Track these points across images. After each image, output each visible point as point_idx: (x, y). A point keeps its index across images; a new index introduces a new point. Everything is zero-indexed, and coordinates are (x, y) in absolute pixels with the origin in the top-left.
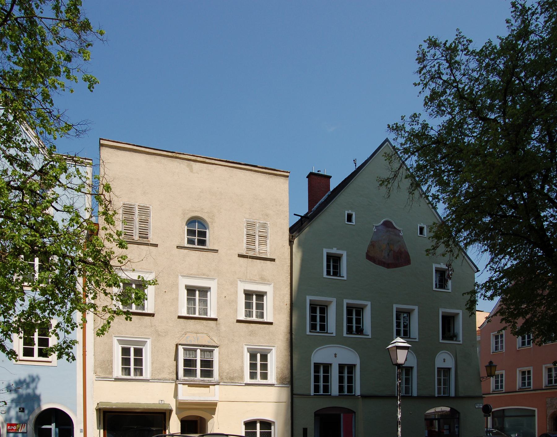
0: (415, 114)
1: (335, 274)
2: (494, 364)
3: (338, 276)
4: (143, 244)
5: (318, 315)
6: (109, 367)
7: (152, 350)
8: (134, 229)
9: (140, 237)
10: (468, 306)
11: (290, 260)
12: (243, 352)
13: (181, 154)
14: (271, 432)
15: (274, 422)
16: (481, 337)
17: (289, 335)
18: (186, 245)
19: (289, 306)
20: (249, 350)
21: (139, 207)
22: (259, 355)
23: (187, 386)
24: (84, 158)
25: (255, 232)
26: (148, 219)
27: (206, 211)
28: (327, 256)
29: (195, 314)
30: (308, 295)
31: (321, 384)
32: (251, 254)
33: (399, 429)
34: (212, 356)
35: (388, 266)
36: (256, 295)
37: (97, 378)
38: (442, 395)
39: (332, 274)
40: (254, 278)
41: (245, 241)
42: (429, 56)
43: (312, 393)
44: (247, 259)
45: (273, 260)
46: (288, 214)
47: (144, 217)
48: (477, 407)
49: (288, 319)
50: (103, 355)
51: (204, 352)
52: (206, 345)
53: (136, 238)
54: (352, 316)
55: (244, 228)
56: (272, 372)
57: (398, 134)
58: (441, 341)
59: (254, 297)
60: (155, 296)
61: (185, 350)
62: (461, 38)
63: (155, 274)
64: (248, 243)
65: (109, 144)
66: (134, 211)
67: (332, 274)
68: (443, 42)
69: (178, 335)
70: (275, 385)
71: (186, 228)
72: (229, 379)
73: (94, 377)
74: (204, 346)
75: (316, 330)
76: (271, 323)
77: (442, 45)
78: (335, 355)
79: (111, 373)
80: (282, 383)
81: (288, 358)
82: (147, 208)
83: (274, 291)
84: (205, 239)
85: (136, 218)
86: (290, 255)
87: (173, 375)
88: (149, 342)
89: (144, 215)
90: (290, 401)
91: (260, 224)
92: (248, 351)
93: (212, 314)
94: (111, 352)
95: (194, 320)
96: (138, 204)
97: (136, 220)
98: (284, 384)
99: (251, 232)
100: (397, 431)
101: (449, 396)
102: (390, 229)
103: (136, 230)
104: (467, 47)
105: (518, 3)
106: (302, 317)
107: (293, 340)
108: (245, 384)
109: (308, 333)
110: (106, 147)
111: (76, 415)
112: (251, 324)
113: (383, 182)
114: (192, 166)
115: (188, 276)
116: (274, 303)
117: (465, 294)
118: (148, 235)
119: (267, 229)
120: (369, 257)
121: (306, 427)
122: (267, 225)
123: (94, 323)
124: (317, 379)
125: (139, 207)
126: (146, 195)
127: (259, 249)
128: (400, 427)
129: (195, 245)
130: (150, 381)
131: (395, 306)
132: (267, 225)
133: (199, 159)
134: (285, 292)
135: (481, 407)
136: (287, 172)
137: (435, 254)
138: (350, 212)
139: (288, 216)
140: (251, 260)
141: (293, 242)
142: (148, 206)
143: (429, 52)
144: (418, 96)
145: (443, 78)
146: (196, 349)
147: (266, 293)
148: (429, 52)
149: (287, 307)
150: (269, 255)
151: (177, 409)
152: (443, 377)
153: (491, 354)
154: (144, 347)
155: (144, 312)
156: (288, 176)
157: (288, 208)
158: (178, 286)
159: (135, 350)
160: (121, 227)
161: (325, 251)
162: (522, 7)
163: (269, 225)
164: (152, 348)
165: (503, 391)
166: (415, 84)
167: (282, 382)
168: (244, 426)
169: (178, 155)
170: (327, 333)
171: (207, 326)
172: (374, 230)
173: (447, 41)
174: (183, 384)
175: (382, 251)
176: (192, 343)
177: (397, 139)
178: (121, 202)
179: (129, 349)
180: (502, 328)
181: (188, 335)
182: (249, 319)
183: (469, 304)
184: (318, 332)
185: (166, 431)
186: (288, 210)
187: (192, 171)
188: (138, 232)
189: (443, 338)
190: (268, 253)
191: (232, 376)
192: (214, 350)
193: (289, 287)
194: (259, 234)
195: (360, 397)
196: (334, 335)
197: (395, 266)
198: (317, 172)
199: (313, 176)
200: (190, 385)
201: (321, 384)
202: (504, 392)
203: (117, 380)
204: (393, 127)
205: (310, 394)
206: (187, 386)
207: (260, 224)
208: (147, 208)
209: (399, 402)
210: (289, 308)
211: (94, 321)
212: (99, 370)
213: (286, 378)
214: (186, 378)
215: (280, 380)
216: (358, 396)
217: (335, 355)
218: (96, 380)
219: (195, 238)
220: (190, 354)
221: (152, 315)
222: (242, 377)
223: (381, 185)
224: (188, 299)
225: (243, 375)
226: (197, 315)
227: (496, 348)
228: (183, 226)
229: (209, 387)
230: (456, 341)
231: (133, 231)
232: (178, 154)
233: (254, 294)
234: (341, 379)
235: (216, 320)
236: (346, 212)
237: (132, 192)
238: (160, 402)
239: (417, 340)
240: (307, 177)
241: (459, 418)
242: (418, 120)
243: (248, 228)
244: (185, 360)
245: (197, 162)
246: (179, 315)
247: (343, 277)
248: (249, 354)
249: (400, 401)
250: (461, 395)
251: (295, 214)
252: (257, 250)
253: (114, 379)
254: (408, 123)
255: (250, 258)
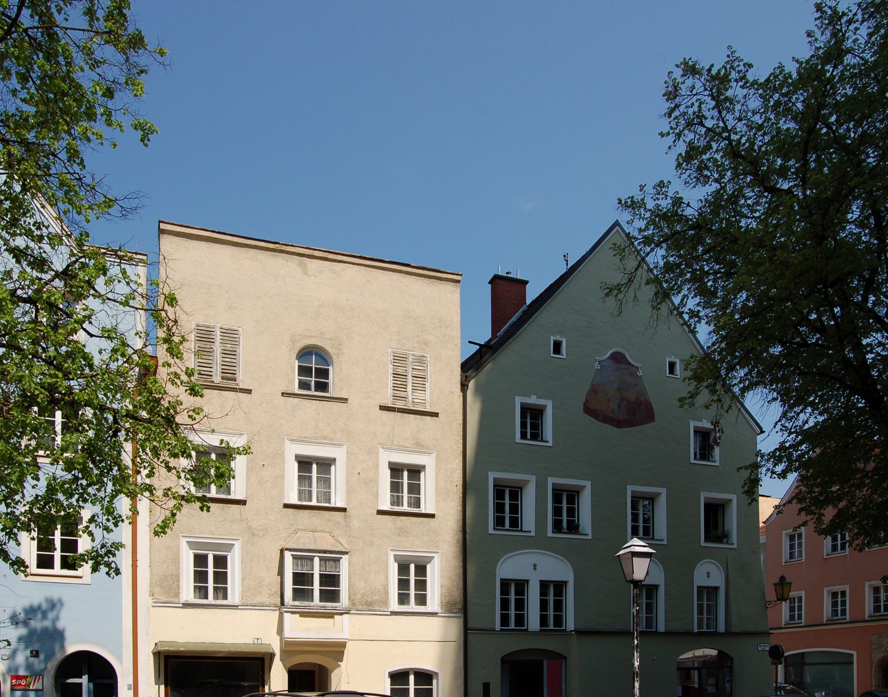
0: (662, 182)
1: (534, 437)
2: (788, 580)
3: (539, 441)
5: (507, 502)
10: (746, 488)
11: (462, 414)
14: (432, 689)
16: (766, 538)
28: (521, 408)
30: (492, 470)
31: (512, 612)
33: (637, 685)
35: (618, 424)
38: (705, 630)
39: (529, 437)
42: (684, 90)
43: (498, 627)
45: (436, 415)
46: (459, 341)
48: (760, 649)
49: (460, 508)
54: (561, 504)
57: (635, 213)
58: (703, 544)
62: (735, 60)
67: (529, 437)
68: (707, 67)
70: (439, 615)
75: (504, 527)
77: (705, 72)
78: (535, 565)
81: (460, 571)
86: (462, 407)
98: (453, 612)
100: (634, 687)
101: (716, 631)
102: (622, 366)
104: (745, 75)
105: (826, 5)
106: (481, 506)
107: (468, 543)
109: (491, 531)
113: (611, 290)
117: (741, 468)
120: (588, 410)
121: (488, 681)
122: (425, 359)
124: (505, 604)
128: (637, 681)
131: (630, 489)
132: (425, 359)
135: (768, 649)
136: (458, 275)
137: (694, 405)
138: (558, 338)
139: (459, 345)
141: (468, 386)
143: (684, 83)
144: (667, 153)
145: (706, 125)
148: (684, 83)
149: (457, 490)
152: (707, 601)
153: (783, 564)
156: (458, 281)
161: (518, 401)
162: (832, 11)
165: (801, 623)
166: (662, 135)
167: (450, 610)
170: (521, 531)
172: (597, 366)
173: (712, 66)
175: (609, 401)
177: (633, 222)
180: (801, 523)
183: (747, 485)
184: (507, 530)
186: (459, 335)
189: (707, 539)
195: (574, 633)
196: (533, 534)
197: (630, 424)
198: (506, 275)
199: (499, 281)
201: (512, 612)
202: (803, 624)
204: (626, 202)
205: (495, 628)
209: (636, 642)
210: (461, 492)
215: (446, 606)
216: (571, 631)
217: (535, 565)
223: (607, 295)
227: (792, 556)
230: (727, 543)
234: (544, 605)
236: (552, 339)
239: (665, 543)
240: (490, 283)
241: (731, 667)
242: (667, 192)
247: (547, 442)
249: (637, 640)
250: (735, 630)
251: (470, 342)
254: (651, 196)
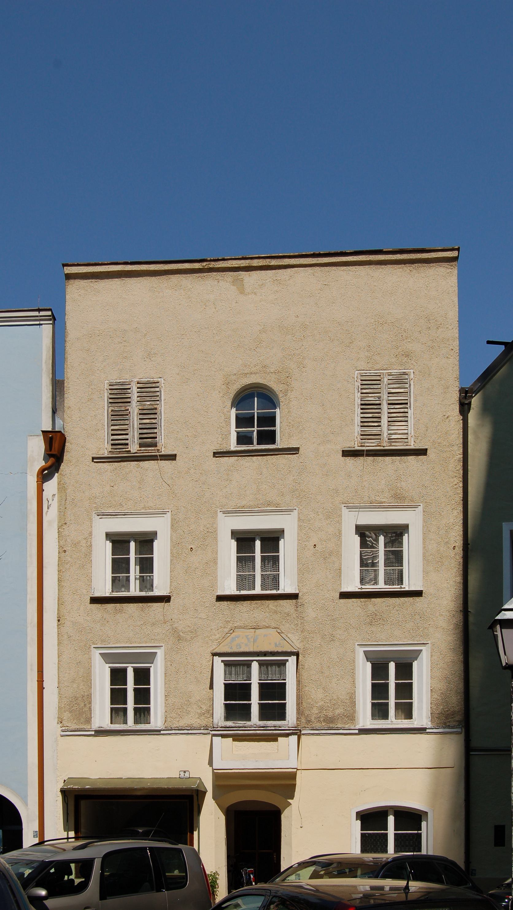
4: (147, 458)
6: (86, 709)
7: (166, 670)
8: (130, 432)
9: (141, 445)
12: (354, 661)
13: (218, 260)
15: (426, 813)
17: (460, 617)
18: (233, 446)
19: (459, 551)
20: (368, 656)
21: (139, 385)
22: (392, 666)
23: (231, 739)
24: (37, 308)
25: (379, 397)
26: (156, 406)
27: (272, 370)
29: (376, 583)
32: (371, 445)
34: (283, 673)
36: (263, 540)
37: (63, 731)
40: (378, 498)
41: (357, 420)
44: (361, 458)
45: (423, 452)
47: (148, 403)
49: (459, 579)
50: (75, 686)
51: (267, 668)
52: (270, 650)
53: (134, 448)
55: (356, 391)
56: (420, 701)
59: (258, 543)
60: (171, 561)
61: (227, 664)
63: (172, 515)
64: (364, 424)
65: (89, 271)
66: (129, 395)
69: (218, 636)
70: (428, 731)
71: (233, 412)
72: (324, 721)
73: (58, 729)
74: (265, 654)
76: (418, 594)
79: (88, 720)
80: (445, 726)
81: (460, 667)
82: (154, 385)
83: (424, 521)
84: (272, 428)
85: (134, 408)
87: (206, 717)
88: (160, 653)
89: (148, 399)
90: (463, 765)
91: (390, 377)
92: (368, 659)
93: (286, 587)
94: (88, 679)
95: (249, 602)
96: (136, 380)
97: (133, 413)
98: (449, 727)
99: (371, 399)
103: (133, 432)
107: (471, 627)
108: (96, 731)
110: (75, 279)
111: (26, 804)
112: (373, 599)
114: (242, 280)
115: (236, 512)
116: (424, 548)
118: (157, 439)
119: (407, 386)
122: (406, 377)
123: (58, 625)
125: (139, 385)
126: (152, 359)
127: (390, 432)
129: (253, 444)
130: (162, 732)
133: (255, 263)
134: (452, 520)
136: (452, 250)
140: (371, 458)
142: (156, 380)
146: (250, 662)
147: (282, 531)
150: (413, 443)
151: (216, 787)
154: (152, 665)
155: (150, 594)
157: (455, 333)
158: (217, 534)
159: (137, 671)
160: (106, 430)
163: (412, 376)
164: (166, 667)
167: (445, 723)
168: (359, 822)
169: (213, 265)
171: (276, 612)
174: (223, 736)
176: (247, 650)
178: (106, 382)
179: (124, 671)
181: (238, 632)
182: (369, 588)
185: (193, 834)
186: (457, 335)
187: (242, 291)
188: (136, 436)
190: (409, 438)
191: (330, 714)
192: (287, 660)
193: (460, 508)
194: (390, 398)
200: (237, 738)
203: (100, 733)
206: (231, 739)
207: (390, 377)
208: (154, 385)
211: (59, 621)
212: (66, 715)
213: (453, 714)
214: (230, 723)
218: (62, 736)
219: (253, 429)
220: (237, 674)
221: (166, 599)
222: (352, 717)
224: (239, 559)
225: (355, 712)
226: (258, 590)
228: (225, 410)
229: (276, 740)
231: (127, 434)
232: (213, 263)
233: (256, 538)
235: (294, 596)
237: (125, 358)
238: (182, 774)
243: (364, 391)
244: (228, 687)
245: (252, 270)
246: (342, 591)
248: (369, 665)
251: (489, 342)
252: (385, 435)
253: (93, 733)
255: (368, 455)
